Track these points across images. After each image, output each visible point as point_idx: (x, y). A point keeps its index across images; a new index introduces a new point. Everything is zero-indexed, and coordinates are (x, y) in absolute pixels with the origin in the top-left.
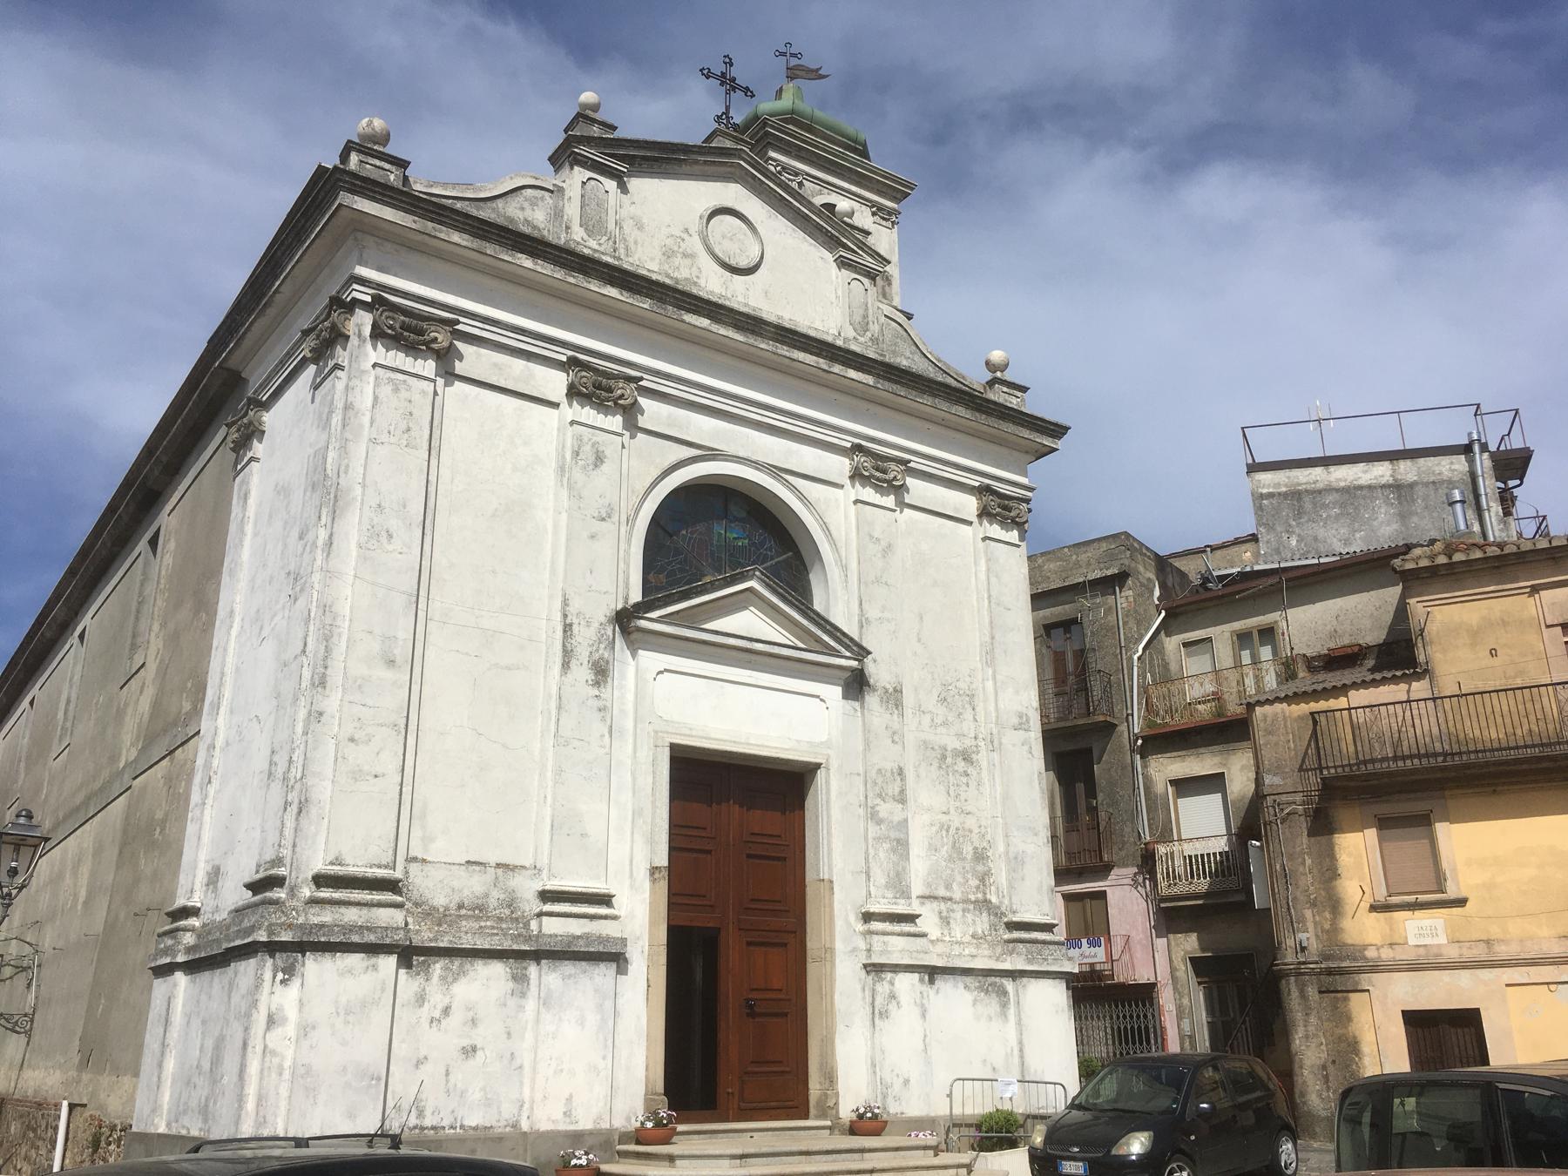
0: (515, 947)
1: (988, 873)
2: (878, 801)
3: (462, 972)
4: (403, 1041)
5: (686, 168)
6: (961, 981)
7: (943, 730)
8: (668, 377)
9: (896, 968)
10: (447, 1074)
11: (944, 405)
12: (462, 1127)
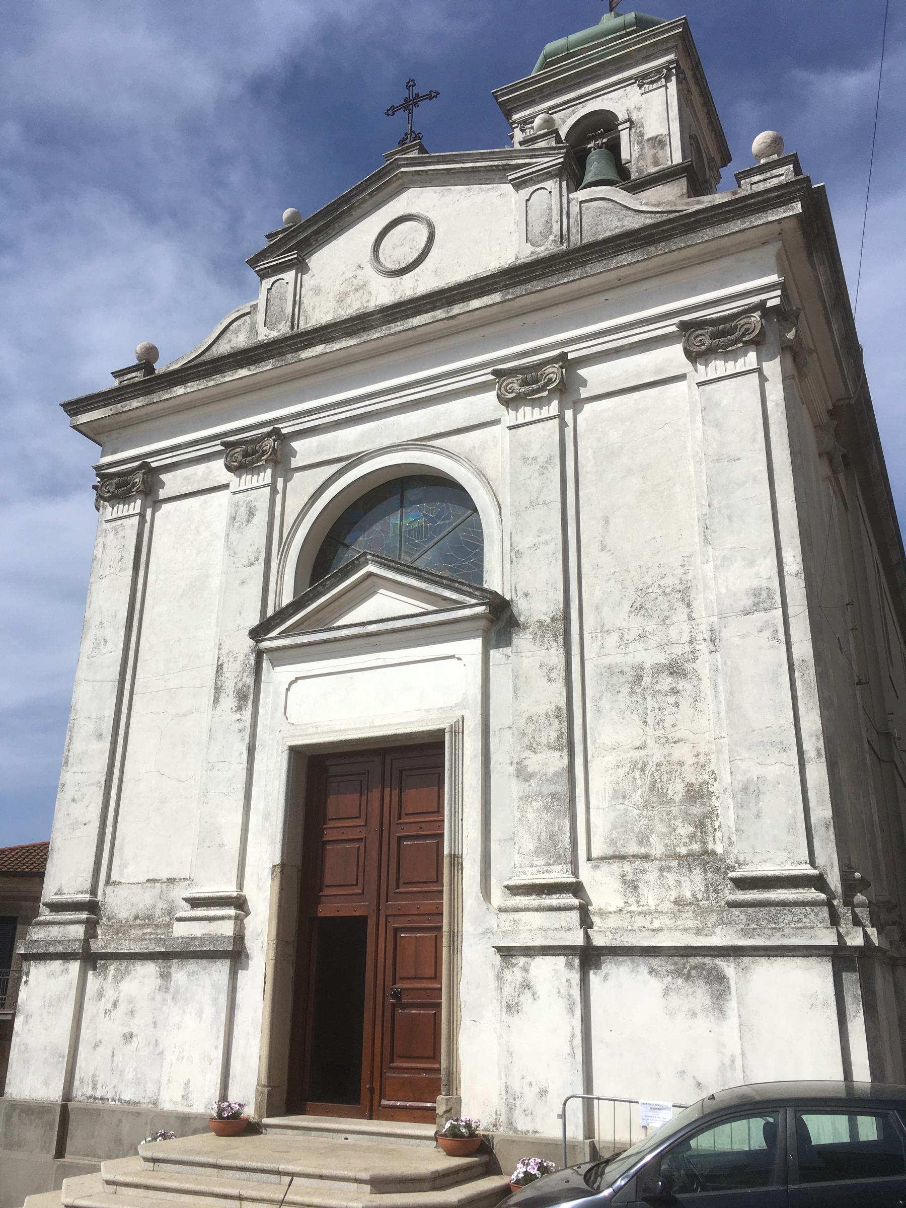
0: (157, 950)
1: (712, 814)
2: (528, 753)
3: (127, 972)
4: (87, 1028)
5: (356, 213)
6: (643, 965)
7: (639, 645)
8: (309, 412)
9: (529, 951)
10: (113, 1056)
11: (599, 267)
12: (120, 1100)
